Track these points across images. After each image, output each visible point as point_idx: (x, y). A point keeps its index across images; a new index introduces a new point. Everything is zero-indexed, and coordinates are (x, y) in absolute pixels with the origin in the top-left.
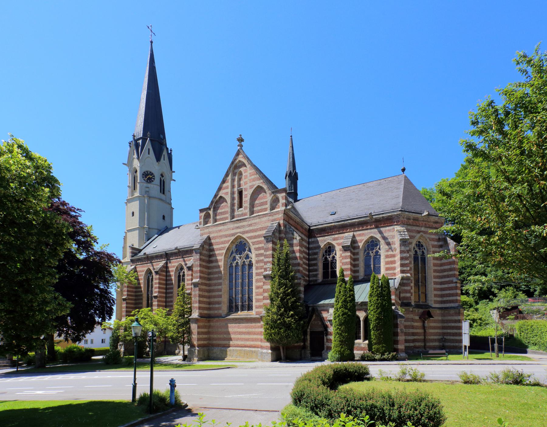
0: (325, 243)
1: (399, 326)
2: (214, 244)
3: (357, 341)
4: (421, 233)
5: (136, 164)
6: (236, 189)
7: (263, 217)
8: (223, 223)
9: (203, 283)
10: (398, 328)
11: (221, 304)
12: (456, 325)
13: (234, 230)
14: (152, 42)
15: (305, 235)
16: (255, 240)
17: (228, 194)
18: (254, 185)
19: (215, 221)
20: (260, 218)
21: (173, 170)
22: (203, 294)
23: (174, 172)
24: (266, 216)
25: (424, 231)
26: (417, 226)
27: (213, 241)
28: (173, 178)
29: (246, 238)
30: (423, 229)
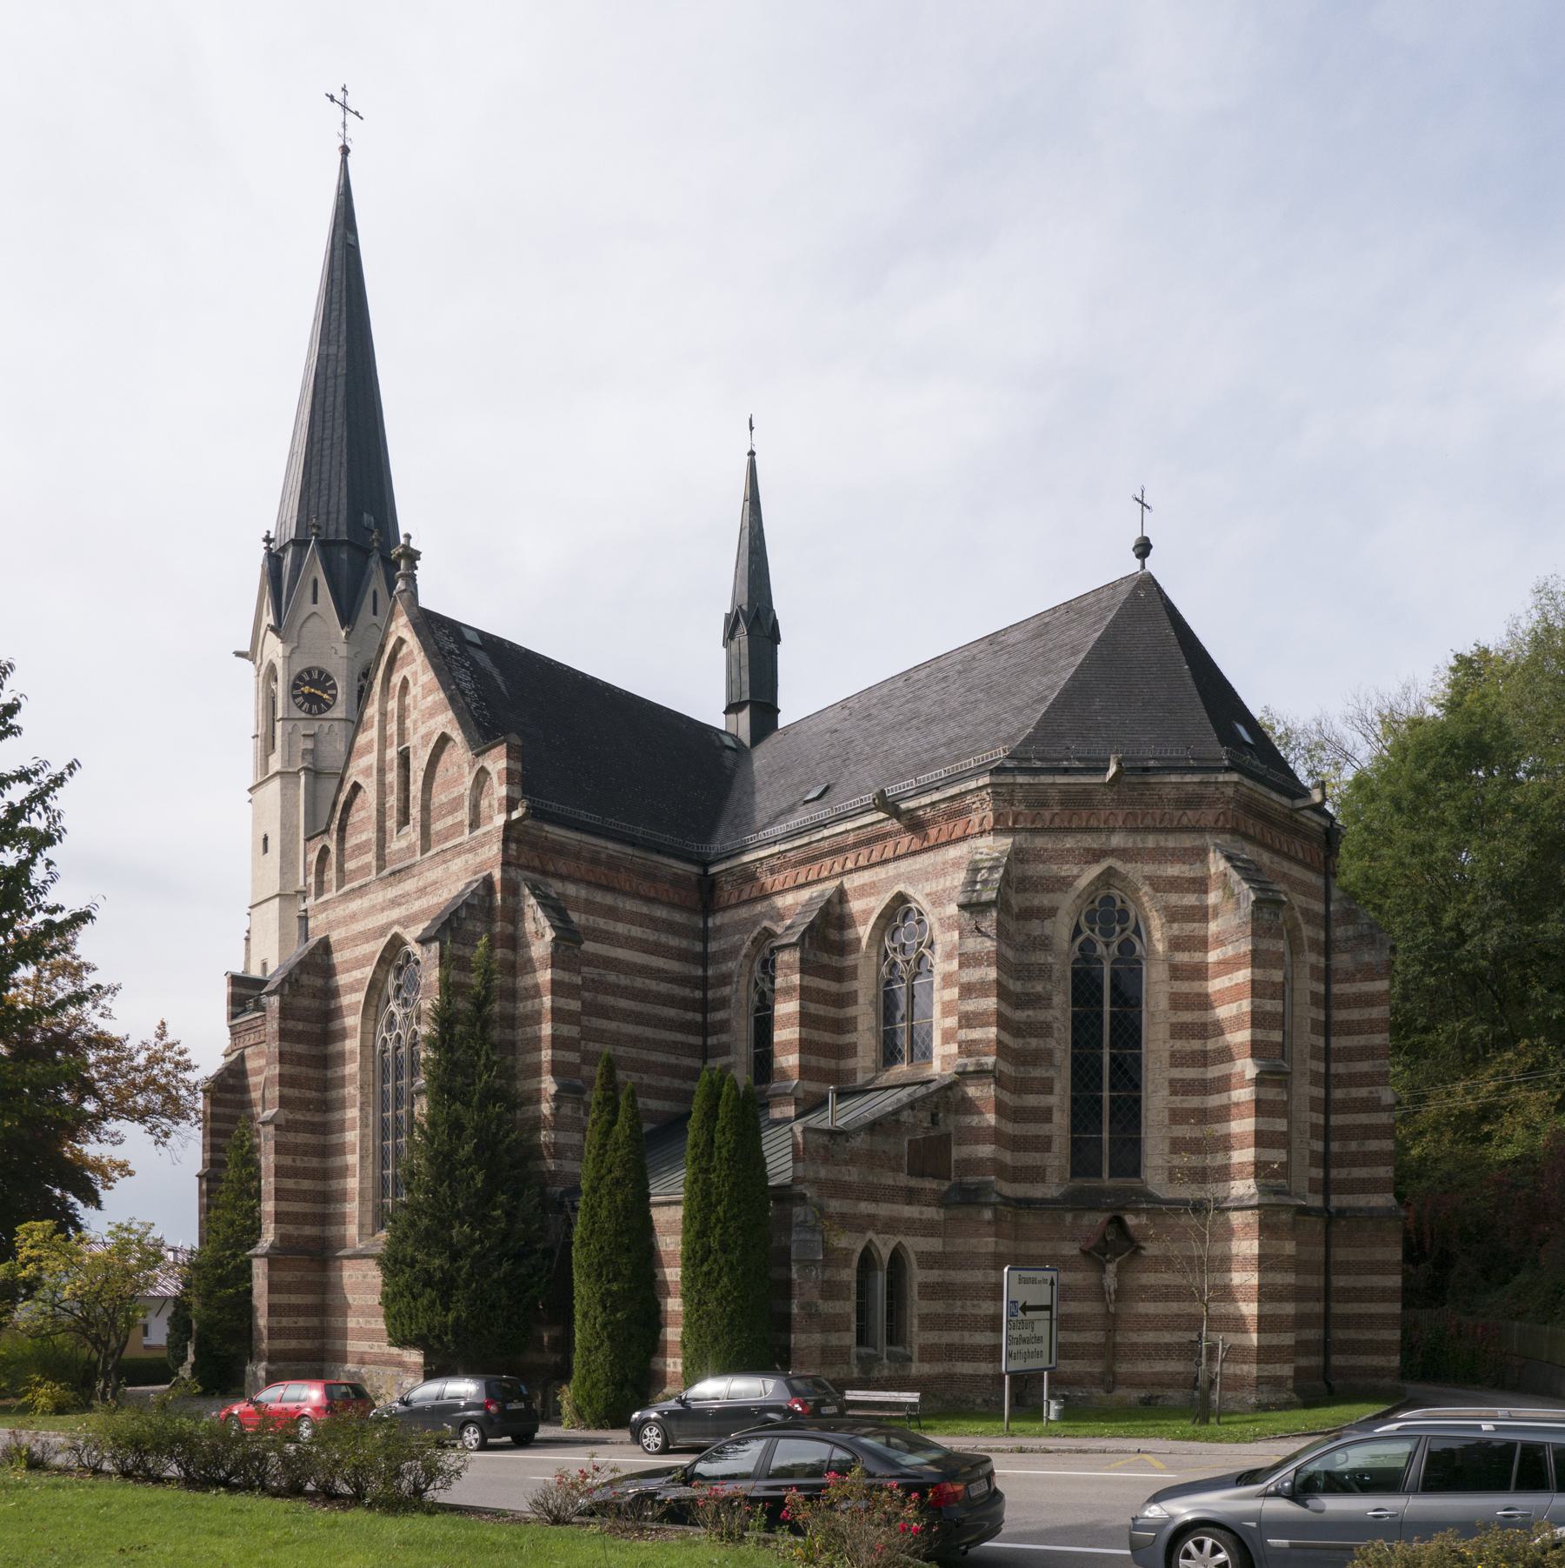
0: (755, 933)
1: (796, 1291)
2: (339, 969)
4: (1108, 862)
5: (274, 648)
6: (392, 753)
8: (361, 887)
9: (296, 1122)
10: (788, 1296)
12: (286, 1322)
13: (385, 913)
14: (345, 151)
15: (672, 905)
17: (371, 775)
19: (341, 883)
20: (445, 862)
22: (299, 1164)
24: (459, 854)
25: (1125, 850)
26: (1097, 830)
27: (338, 958)
30: (1117, 840)
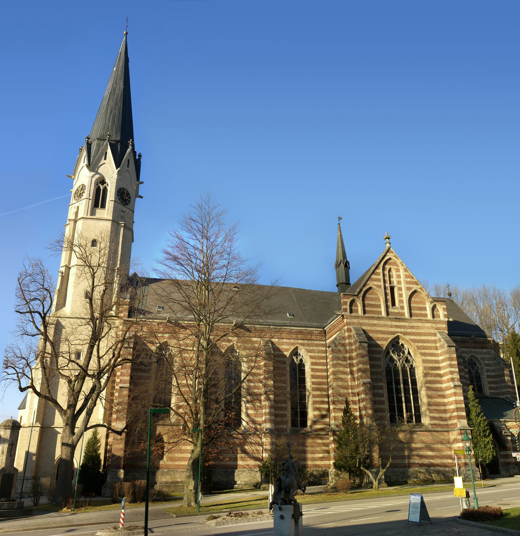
3: (259, 469)
7: (426, 323)
11: (385, 412)
16: (420, 344)
18: (412, 288)
21: (141, 180)
23: (142, 183)
28: (140, 194)
29: (479, 359)
